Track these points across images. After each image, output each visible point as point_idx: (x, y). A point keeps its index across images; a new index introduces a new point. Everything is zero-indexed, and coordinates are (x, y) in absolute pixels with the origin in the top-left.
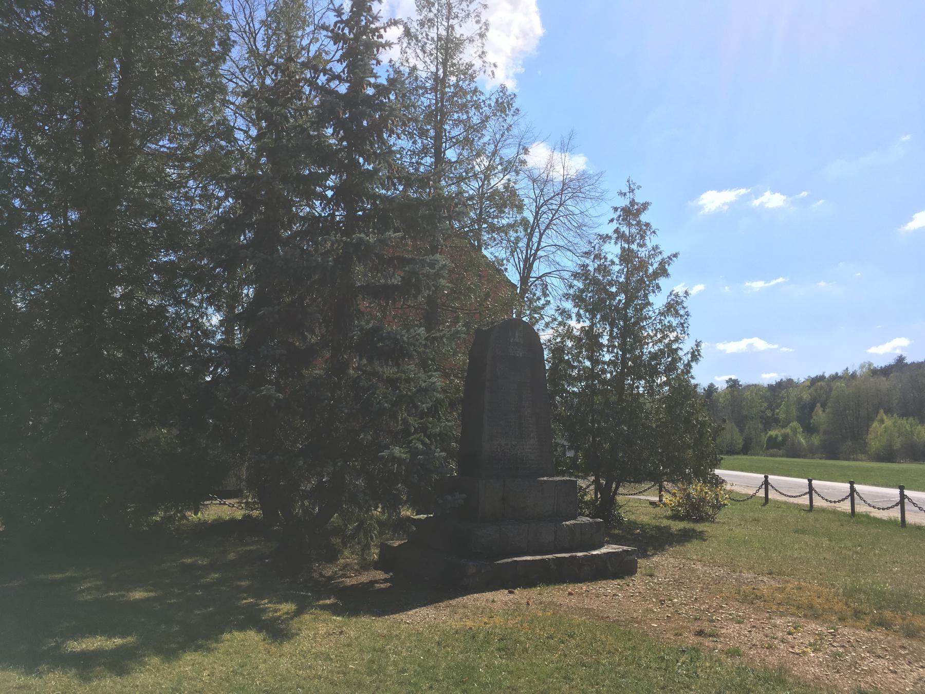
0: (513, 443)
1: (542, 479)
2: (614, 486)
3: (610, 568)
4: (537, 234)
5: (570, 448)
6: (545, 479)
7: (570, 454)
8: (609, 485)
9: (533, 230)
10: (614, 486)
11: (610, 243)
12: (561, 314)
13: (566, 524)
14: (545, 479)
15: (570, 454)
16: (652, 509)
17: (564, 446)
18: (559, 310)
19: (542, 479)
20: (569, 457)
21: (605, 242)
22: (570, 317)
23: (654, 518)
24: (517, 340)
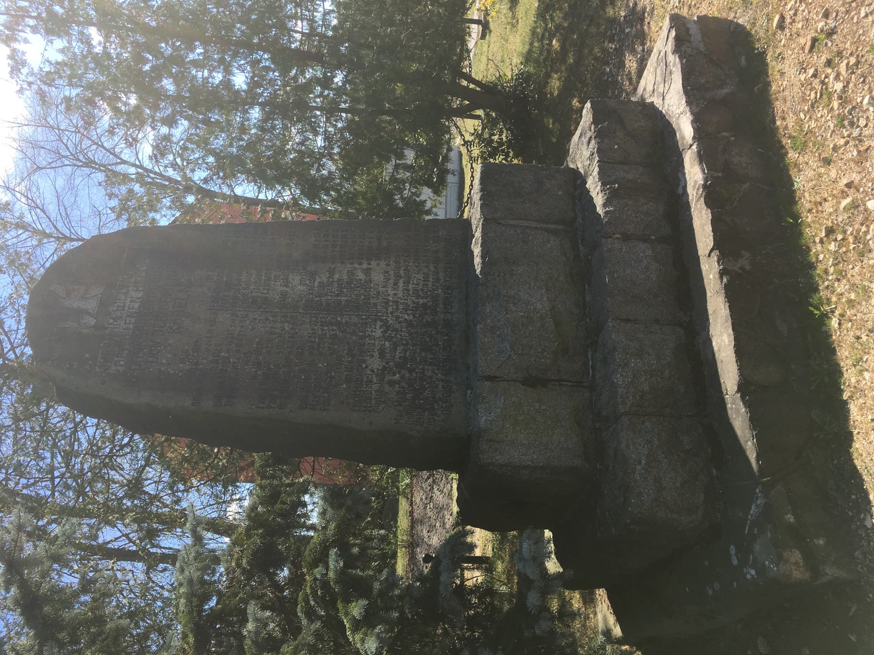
0: (378, 333)
1: (477, 260)
2: (464, 83)
3: (726, 91)
4: (121, 168)
5: (401, 156)
6: (477, 250)
7: (410, 156)
8: (465, 93)
9: (116, 174)
10: (464, 83)
11: (23, 53)
12: (163, 155)
13: (605, 205)
14: (477, 250)
15: (410, 156)
16: (492, 34)
17: (397, 167)
18: (156, 156)
19: (477, 260)
20: (416, 159)
21: (24, 63)
22: (167, 138)
23: (513, 26)
24: (92, 305)
